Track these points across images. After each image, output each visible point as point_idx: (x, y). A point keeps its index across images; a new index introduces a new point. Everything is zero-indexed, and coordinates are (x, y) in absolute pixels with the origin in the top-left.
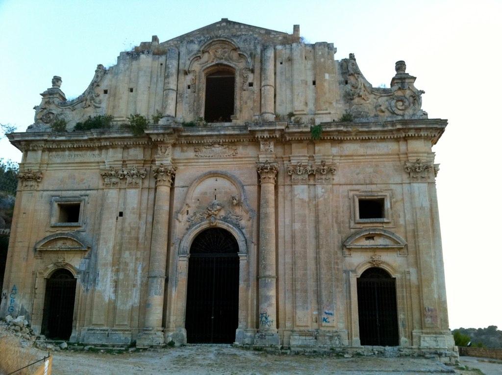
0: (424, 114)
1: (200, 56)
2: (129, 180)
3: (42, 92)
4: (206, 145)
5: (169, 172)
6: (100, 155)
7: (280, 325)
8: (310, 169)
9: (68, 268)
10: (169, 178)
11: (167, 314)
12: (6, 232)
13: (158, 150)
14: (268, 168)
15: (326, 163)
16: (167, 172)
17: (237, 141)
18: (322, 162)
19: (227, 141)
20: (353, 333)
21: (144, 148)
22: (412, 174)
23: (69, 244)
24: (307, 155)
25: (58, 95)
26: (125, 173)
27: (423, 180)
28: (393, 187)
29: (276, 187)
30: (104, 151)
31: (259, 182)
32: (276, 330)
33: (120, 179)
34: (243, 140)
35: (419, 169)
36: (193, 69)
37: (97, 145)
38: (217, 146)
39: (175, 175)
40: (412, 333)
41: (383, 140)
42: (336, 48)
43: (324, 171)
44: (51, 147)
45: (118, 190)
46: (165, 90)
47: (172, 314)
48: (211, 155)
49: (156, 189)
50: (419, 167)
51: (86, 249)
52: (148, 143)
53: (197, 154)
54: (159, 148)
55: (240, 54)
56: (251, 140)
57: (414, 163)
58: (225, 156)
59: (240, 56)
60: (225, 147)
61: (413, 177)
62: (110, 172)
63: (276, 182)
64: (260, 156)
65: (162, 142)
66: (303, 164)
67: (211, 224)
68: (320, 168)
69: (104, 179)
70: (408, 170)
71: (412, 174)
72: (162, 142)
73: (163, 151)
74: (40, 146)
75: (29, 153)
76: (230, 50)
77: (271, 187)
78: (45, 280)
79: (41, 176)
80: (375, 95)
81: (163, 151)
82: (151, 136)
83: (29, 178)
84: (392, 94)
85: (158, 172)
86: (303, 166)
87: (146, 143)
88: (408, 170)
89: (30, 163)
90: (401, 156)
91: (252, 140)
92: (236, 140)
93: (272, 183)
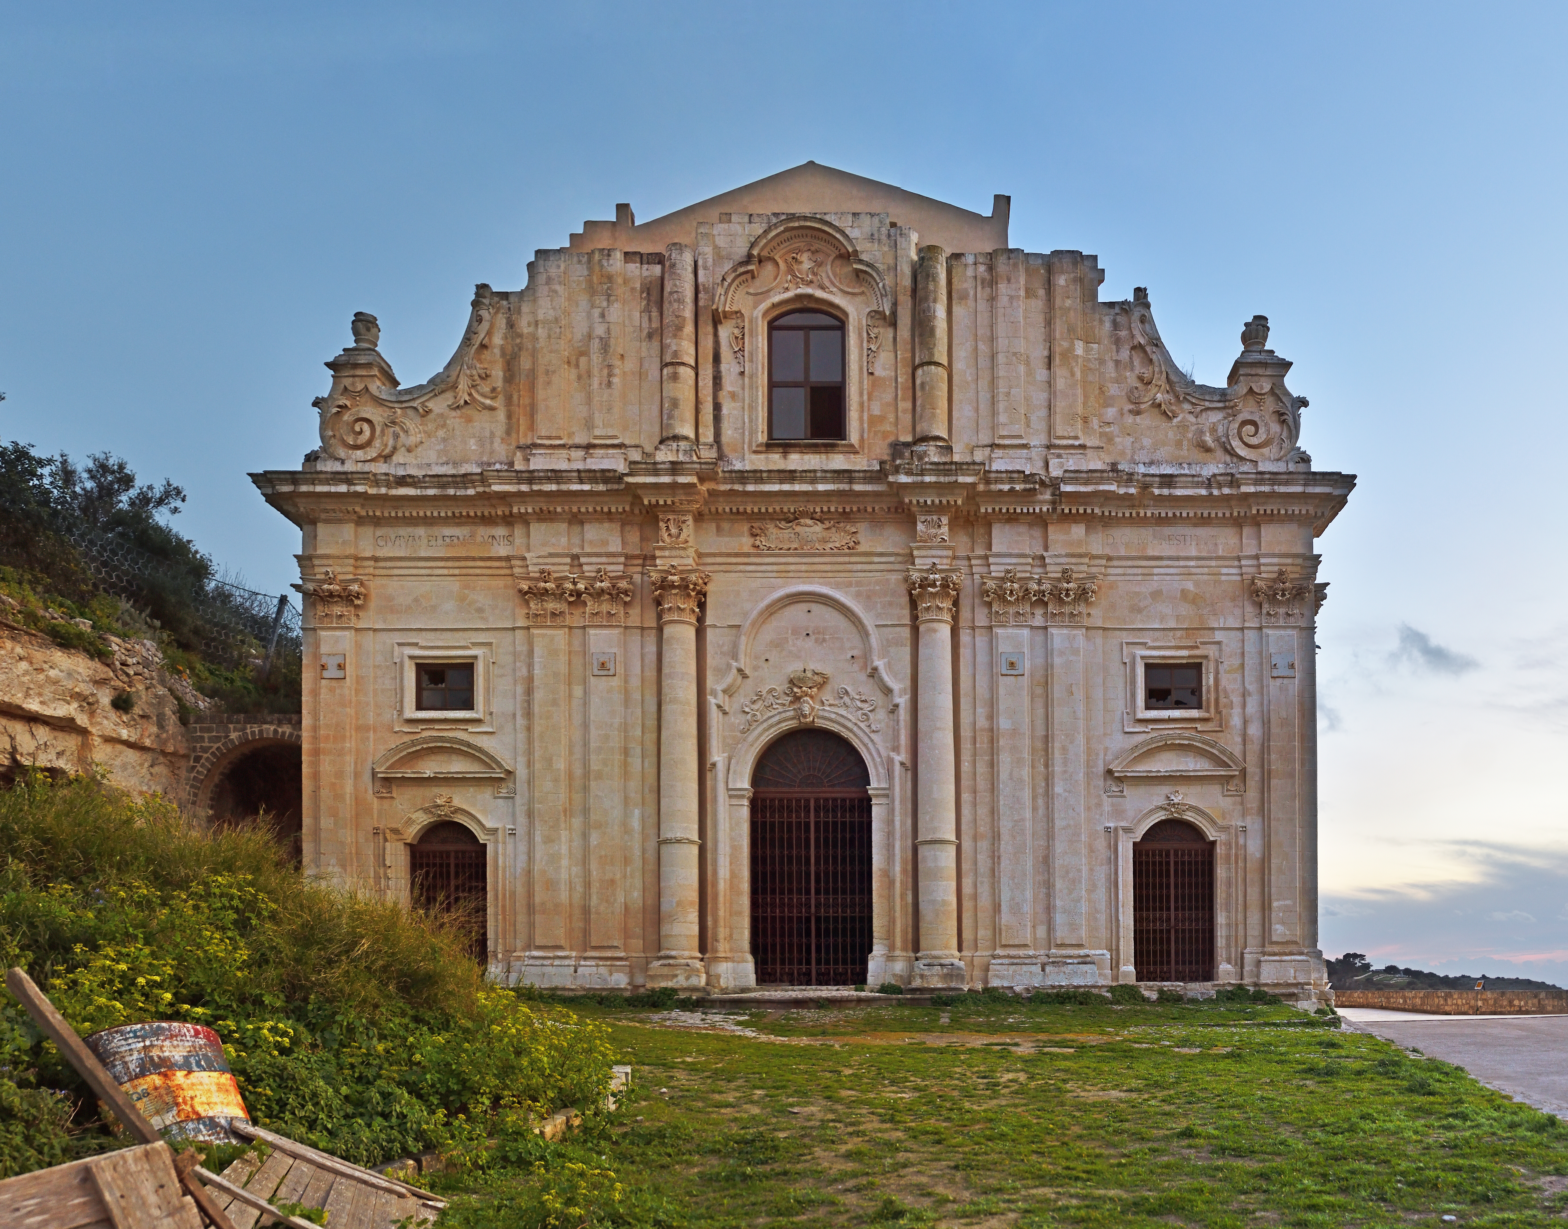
0: (1302, 459)
1: (752, 271)
2: (591, 606)
3: (330, 359)
4: (780, 520)
5: (691, 586)
6: (509, 538)
7: (965, 945)
8: (1036, 587)
9: (460, 819)
10: (692, 604)
11: (710, 923)
12: (284, 733)
13: (658, 528)
14: (938, 583)
15: (1075, 576)
16: (687, 587)
17: (859, 510)
18: (1064, 572)
19: (833, 509)
20: (1122, 957)
21: (623, 525)
22: (1266, 607)
23: (458, 766)
24: (1027, 552)
25: (375, 371)
26: (581, 586)
27: (559, 620)
28: (1219, 636)
29: (955, 632)
30: (519, 531)
31: (915, 618)
32: (957, 953)
33: (570, 603)
34: (873, 509)
35: (1283, 595)
36: (735, 308)
37: (500, 513)
38: (809, 522)
39: (705, 595)
40: (1242, 954)
41: (1204, 521)
42: (1103, 270)
43: (1067, 595)
44: (378, 513)
45: (622, 630)
46: (664, 365)
47: (721, 923)
48: (786, 547)
49: (660, 630)
50: (1283, 590)
51: (502, 776)
52: (632, 511)
53: (758, 543)
54: (662, 525)
55: (858, 272)
56: (893, 510)
57: (1274, 580)
58: (828, 551)
59: (858, 276)
60: (827, 524)
61: (1268, 614)
62: (542, 584)
63: (955, 618)
64: (915, 553)
65: (669, 508)
66: (1019, 575)
67: (802, 720)
68: (1060, 585)
69: (527, 602)
70: (1258, 595)
71: (1266, 607)
72: (669, 508)
73: (674, 531)
74: (350, 509)
75: (322, 530)
76: (831, 258)
77: (945, 631)
78: (408, 848)
79: (362, 590)
80: (1193, 404)
81: (674, 531)
82: (639, 492)
83: (331, 594)
84: (1232, 404)
85: (664, 586)
86: (1020, 579)
87: (627, 508)
88: (1258, 595)
89: (327, 557)
90: (973, 562)
91: (896, 509)
92: (855, 509)
93: (946, 622)
